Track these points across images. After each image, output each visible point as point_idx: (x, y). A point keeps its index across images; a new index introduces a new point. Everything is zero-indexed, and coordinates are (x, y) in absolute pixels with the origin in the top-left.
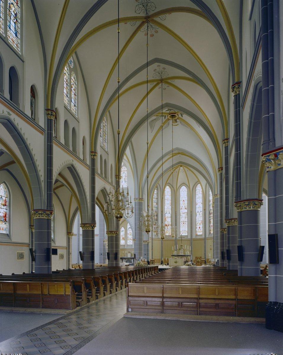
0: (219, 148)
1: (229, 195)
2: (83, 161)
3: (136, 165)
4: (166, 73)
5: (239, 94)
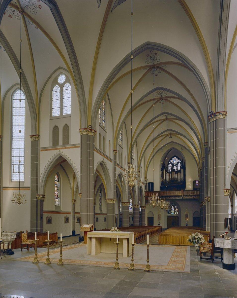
0: (205, 125)
1: (208, 174)
2: (108, 158)
3: (126, 132)
4: (158, 58)
5: (207, 147)
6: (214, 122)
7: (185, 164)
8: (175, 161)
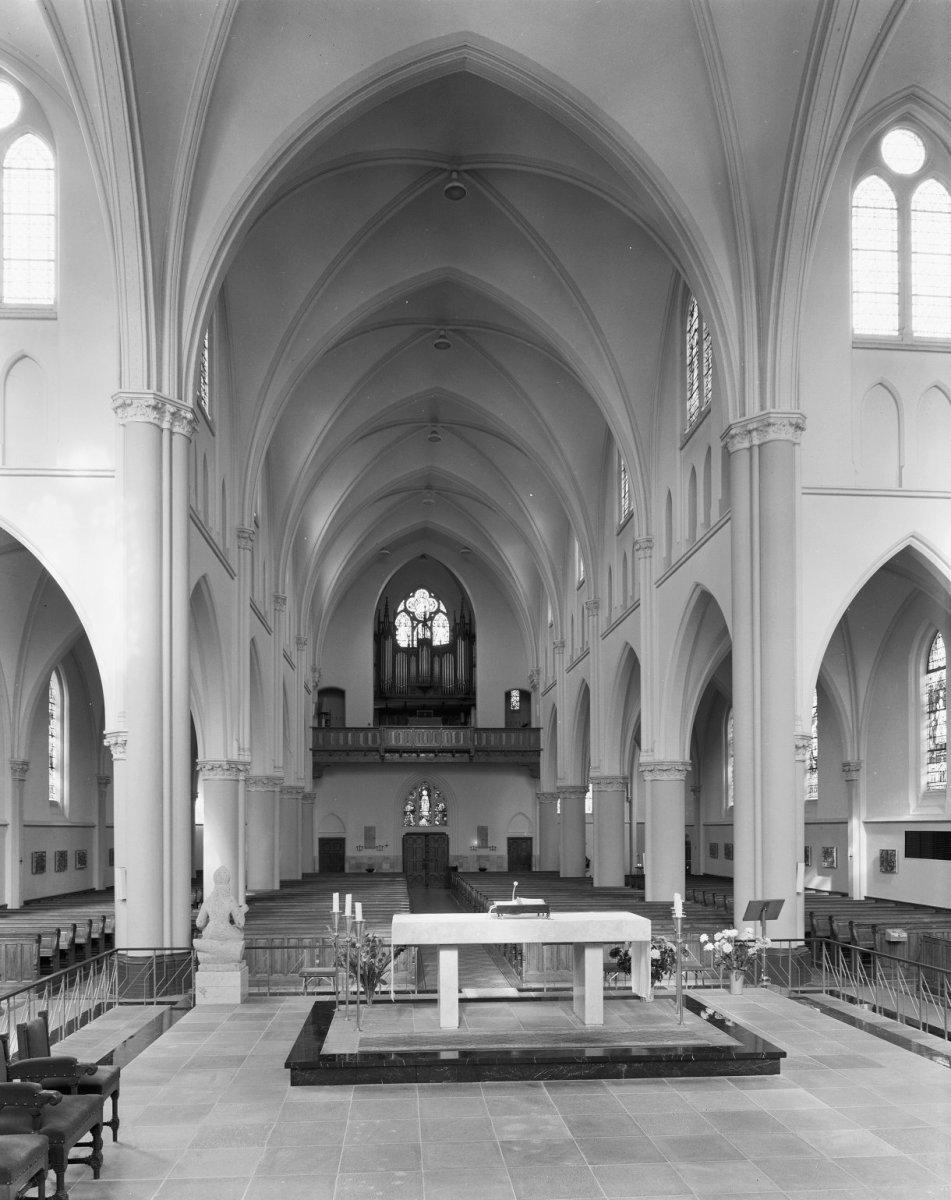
6: (756, 451)
7: (470, 620)
8: (422, 602)
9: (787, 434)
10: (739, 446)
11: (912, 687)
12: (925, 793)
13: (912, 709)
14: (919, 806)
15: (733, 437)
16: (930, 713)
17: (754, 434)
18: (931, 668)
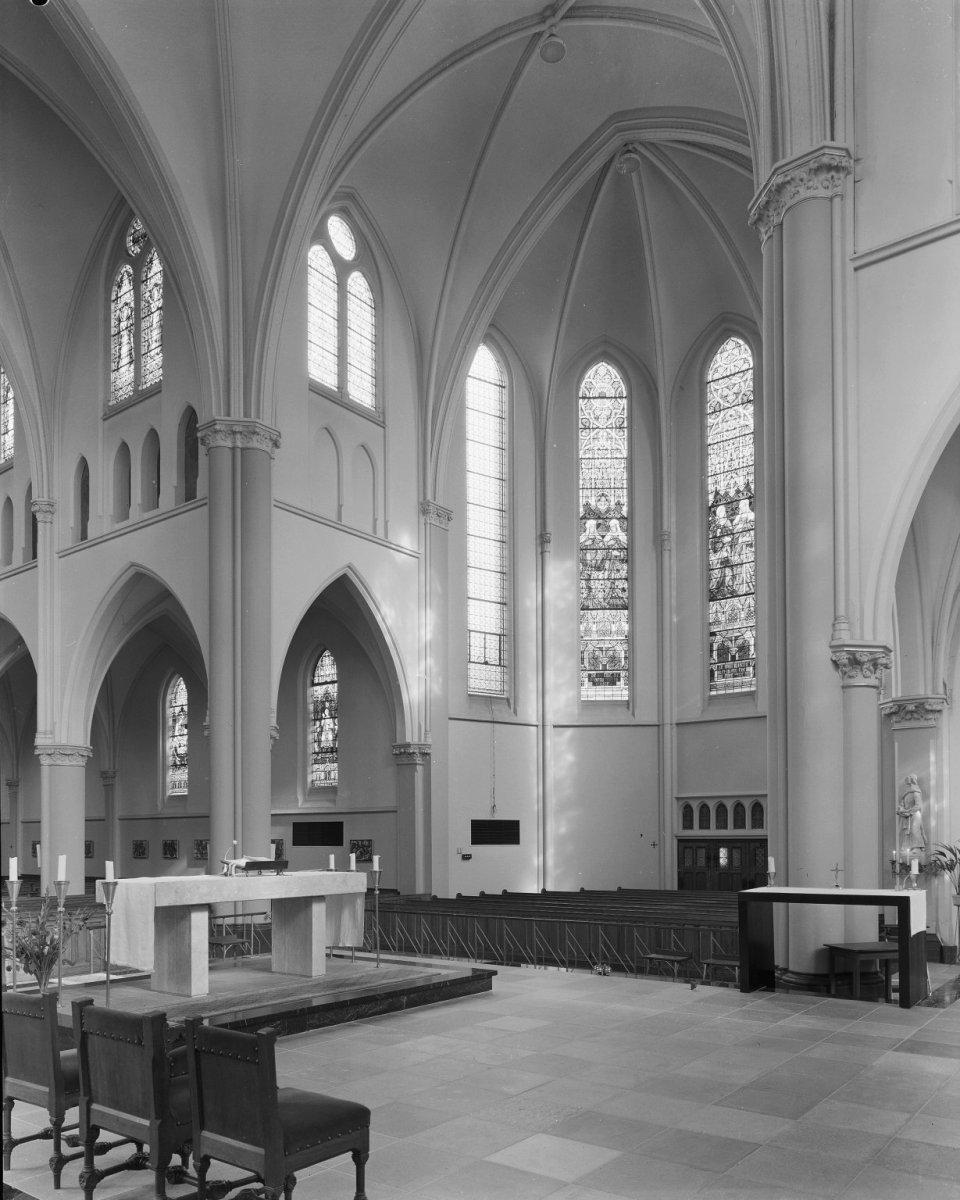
9: (266, 446)
10: (222, 443)
11: (300, 696)
12: (310, 789)
13: (300, 720)
14: (305, 801)
15: (216, 432)
16: (315, 720)
17: (238, 436)
18: (316, 681)
